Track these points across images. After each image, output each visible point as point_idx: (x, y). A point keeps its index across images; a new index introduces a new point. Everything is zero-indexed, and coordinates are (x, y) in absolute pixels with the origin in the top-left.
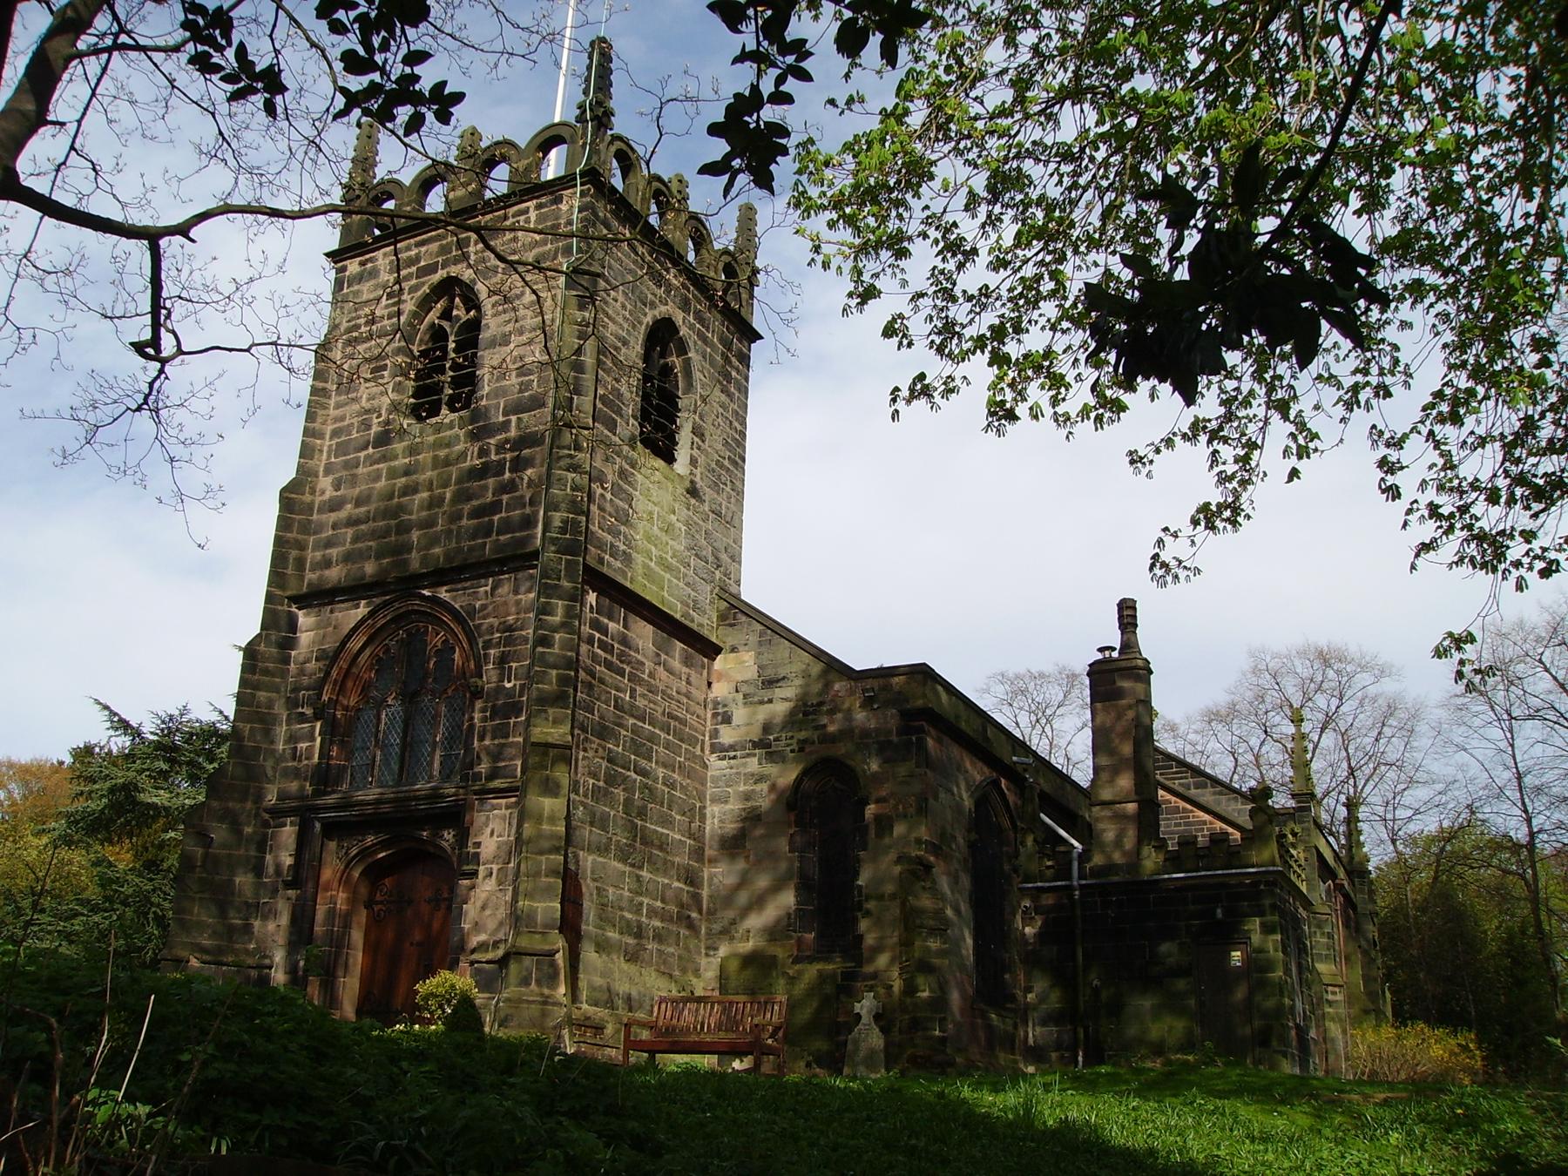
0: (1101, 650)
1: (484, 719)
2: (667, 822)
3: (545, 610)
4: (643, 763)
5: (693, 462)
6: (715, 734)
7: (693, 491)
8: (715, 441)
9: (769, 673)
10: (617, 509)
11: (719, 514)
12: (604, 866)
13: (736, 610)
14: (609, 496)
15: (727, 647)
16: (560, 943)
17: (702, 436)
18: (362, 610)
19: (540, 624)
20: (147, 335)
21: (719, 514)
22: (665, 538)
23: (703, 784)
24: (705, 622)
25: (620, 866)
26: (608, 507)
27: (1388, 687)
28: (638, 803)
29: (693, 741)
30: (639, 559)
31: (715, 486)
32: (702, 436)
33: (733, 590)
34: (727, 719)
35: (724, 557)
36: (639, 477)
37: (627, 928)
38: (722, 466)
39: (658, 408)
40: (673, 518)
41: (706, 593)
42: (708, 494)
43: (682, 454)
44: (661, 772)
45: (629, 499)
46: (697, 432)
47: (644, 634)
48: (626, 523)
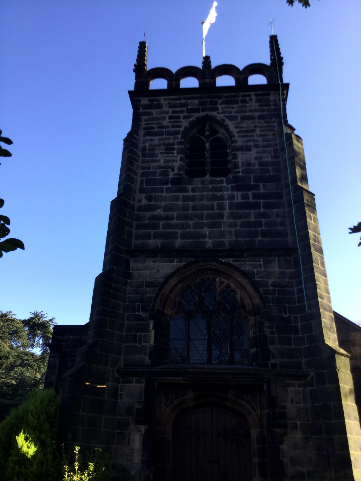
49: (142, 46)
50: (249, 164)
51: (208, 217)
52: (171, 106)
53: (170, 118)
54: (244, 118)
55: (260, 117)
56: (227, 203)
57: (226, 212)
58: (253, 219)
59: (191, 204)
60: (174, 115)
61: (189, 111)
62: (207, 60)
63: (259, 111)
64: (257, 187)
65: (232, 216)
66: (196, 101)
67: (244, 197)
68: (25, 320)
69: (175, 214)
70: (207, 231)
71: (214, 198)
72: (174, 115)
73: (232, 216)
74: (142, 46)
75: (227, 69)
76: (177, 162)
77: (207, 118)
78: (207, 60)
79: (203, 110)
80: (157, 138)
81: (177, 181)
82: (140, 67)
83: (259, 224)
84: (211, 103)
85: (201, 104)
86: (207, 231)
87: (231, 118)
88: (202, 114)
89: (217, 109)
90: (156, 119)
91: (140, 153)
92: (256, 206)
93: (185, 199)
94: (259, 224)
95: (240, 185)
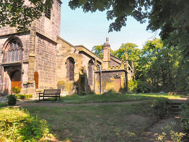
0: (104, 43)
1: (24, 53)
2: (50, 65)
3: (31, 38)
4: (47, 58)
5: (53, 19)
6: (57, 54)
7: (53, 23)
8: (56, 16)
9: (63, 46)
10: (42, 25)
11: (57, 26)
12: (41, 71)
13: (58, 38)
14: (40, 23)
15: (58, 43)
16: (34, 81)
17: (54, 16)
18: (7, 39)
19: (30, 40)
20: (89, 59)
21: (57, 26)
22: (49, 29)
23: (55, 60)
24: (55, 40)
25: (44, 71)
26: (40, 25)
27: (137, 48)
28: (46, 63)
29: (54, 55)
30: (45, 31)
31: (56, 23)
32: (54, 16)
33: (59, 36)
34: (58, 52)
35: (58, 32)
36: (45, 21)
37: (45, 78)
38: (57, 20)
39: (48, 14)
40: (50, 26)
41: (55, 36)
42: (55, 23)
43: (51, 18)
44: (49, 59)
45: (43, 24)
46: (54, 15)
47: (46, 42)
48: (43, 26)
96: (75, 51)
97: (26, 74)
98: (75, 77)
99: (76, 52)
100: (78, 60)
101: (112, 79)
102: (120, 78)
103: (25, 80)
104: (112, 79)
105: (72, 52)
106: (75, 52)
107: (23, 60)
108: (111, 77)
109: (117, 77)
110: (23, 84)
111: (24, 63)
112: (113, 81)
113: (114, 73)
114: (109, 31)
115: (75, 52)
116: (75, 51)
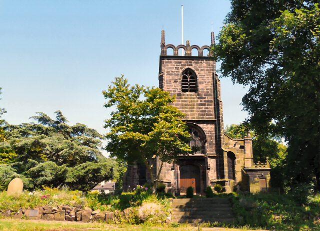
49: (163, 33)
50: (203, 89)
51: (190, 108)
52: (175, 63)
53: (176, 68)
54: (202, 70)
55: (207, 70)
56: (195, 103)
57: (195, 107)
58: (203, 110)
59: (184, 103)
60: (225, 155)
61: (182, 65)
62: (188, 42)
63: (206, 67)
64: (205, 98)
65: (197, 108)
66: (184, 61)
67: (201, 101)
68: (262, 227)
69: (179, 107)
70: (189, 113)
71: (192, 101)
72: (225, 155)
73: (197, 108)
74: (163, 33)
75: (195, 47)
76: (179, 87)
77: (189, 69)
78: (188, 42)
79: (187, 65)
80: (171, 76)
81: (179, 94)
82: (163, 46)
83: (205, 111)
84: (190, 62)
85: (187, 62)
86: (189, 113)
87: (198, 70)
88: (187, 67)
89: (192, 65)
90: (170, 68)
91: (165, 82)
92: (205, 105)
93: (183, 101)
94: (205, 111)
95: (200, 98)
96: (235, 145)
97: (213, 170)
98: (236, 176)
99: (236, 146)
100: (240, 156)
101: (256, 179)
102: (266, 178)
103: (212, 177)
104: (256, 179)
105: (231, 146)
106: (234, 146)
107: (208, 154)
108: (256, 177)
109: (262, 177)
110: (209, 182)
111: (210, 157)
112: (258, 182)
113: (259, 173)
114: (104, 93)
115: (234, 146)
116: (235, 145)
